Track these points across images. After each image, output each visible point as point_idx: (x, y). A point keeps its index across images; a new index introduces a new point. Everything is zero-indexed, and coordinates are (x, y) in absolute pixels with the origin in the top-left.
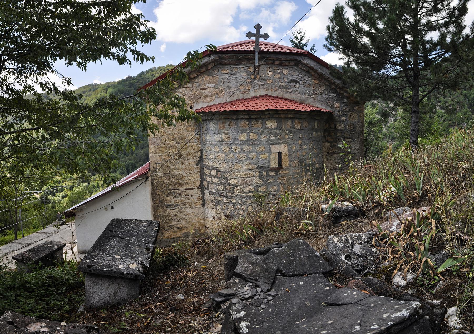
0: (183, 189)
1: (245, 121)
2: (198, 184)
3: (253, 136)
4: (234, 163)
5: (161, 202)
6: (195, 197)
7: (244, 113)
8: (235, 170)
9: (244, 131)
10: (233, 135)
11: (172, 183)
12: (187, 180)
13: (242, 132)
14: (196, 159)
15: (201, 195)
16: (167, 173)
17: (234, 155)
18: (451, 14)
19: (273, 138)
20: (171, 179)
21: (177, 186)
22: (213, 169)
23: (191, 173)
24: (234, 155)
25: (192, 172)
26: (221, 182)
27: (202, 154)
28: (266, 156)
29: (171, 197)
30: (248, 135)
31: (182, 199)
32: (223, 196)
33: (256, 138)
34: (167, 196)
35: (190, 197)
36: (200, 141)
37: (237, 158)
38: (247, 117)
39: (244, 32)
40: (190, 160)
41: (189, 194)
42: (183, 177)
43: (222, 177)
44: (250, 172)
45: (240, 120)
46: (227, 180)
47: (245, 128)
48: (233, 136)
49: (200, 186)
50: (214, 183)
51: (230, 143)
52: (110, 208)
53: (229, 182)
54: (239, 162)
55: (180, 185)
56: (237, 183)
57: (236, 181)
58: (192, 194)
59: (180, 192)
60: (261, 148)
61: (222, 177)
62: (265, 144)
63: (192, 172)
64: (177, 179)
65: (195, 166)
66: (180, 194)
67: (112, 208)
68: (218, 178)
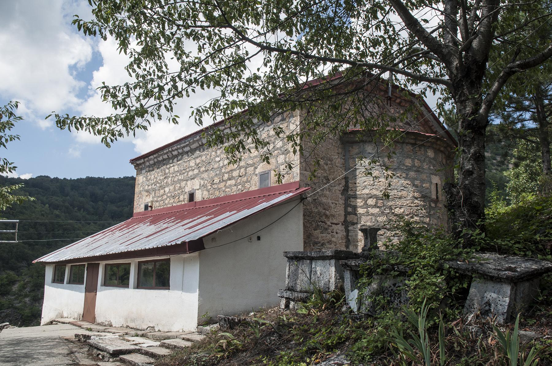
0: (329, 223)
1: (410, 146)
2: (342, 219)
3: (417, 163)
4: (399, 190)
5: (309, 238)
6: (339, 235)
7: (413, 137)
8: (400, 198)
9: (408, 157)
10: (398, 159)
11: (319, 213)
12: (333, 211)
13: (407, 157)
14: (341, 187)
15: (345, 234)
16: (315, 200)
17: (399, 181)
18: (204, 30)
19: (432, 168)
20: (319, 207)
21: (323, 219)
22: (370, 198)
23: (336, 204)
24: (399, 181)
25: (337, 202)
26: (383, 212)
27: (347, 182)
28: (428, 185)
29: (318, 231)
30: (413, 160)
31: (329, 236)
32: (385, 228)
33: (420, 165)
34: (315, 230)
35: (335, 234)
36: (346, 168)
37: (402, 184)
38: (412, 141)
39: (92, 39)
40: (336, 188)
41: (335, 231)
42: (330, 207)
43: (384, 206)
44: (416, 201)
45: (405, 145)
46: (392, 209)
47: (409, 153)
48: (399, 161)
49: (344, 222)
50: (372, 214)
51: (395, 167)
52: (256, 238)
53: (393, 211)
54: (405, 189)
55: (327, 216)
56: (404, 212)
57: (402, 210)
58: (338, 231)
59: (326, 226)
60: (424, 176)
61: (384, 206)
62: (427, 173)
63: (337, 202)
64: (325, 209)
65: (340, 196)
66: (326, 229)
67: (259, 238)
68: (378, 207)
